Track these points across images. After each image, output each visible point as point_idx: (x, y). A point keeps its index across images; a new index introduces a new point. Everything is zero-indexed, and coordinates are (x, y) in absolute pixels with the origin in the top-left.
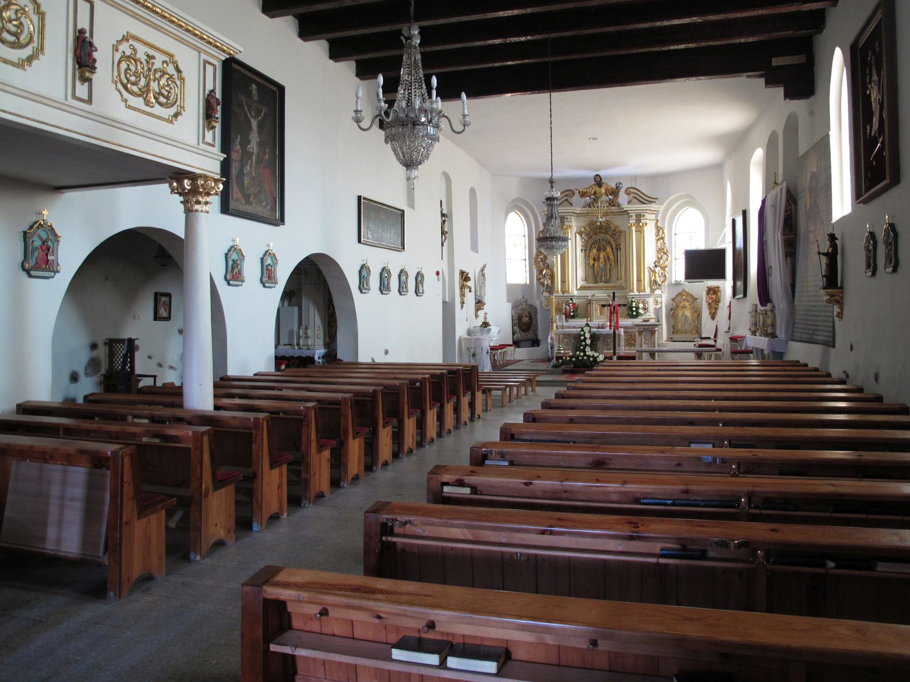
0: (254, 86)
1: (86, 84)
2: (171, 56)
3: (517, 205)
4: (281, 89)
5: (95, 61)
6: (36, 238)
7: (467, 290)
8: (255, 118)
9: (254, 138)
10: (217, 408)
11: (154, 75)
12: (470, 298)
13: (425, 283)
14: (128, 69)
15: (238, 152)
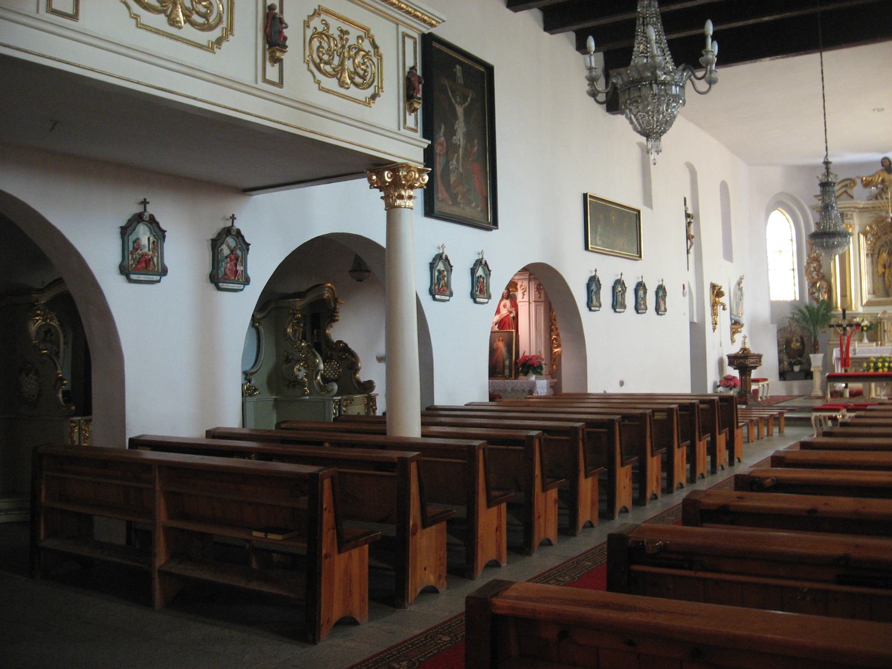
0: (458, 67)
1: (277, 65)
2: (367, 30)
4: (490, 69)
5: (285, 39)
6: (224, 247)
7: (720, 308)
8: (461, 104)
9: (460, 127)
11: (349, 52)
12: (724, 318)
13: (667, 299)
14: (320, 46)
15: (442, 144)
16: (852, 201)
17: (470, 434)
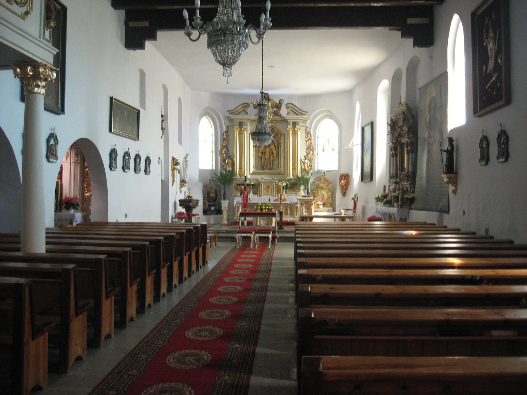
3: (208, 113)
10: (47, 251)
16: (247, 116)
17: (80, 250)
